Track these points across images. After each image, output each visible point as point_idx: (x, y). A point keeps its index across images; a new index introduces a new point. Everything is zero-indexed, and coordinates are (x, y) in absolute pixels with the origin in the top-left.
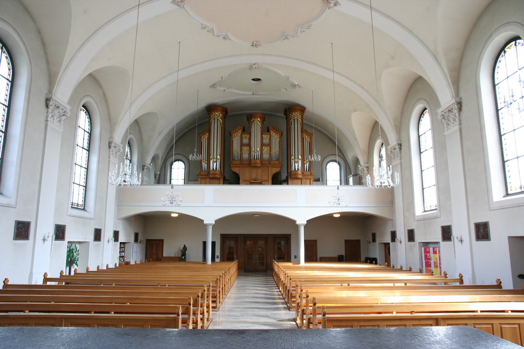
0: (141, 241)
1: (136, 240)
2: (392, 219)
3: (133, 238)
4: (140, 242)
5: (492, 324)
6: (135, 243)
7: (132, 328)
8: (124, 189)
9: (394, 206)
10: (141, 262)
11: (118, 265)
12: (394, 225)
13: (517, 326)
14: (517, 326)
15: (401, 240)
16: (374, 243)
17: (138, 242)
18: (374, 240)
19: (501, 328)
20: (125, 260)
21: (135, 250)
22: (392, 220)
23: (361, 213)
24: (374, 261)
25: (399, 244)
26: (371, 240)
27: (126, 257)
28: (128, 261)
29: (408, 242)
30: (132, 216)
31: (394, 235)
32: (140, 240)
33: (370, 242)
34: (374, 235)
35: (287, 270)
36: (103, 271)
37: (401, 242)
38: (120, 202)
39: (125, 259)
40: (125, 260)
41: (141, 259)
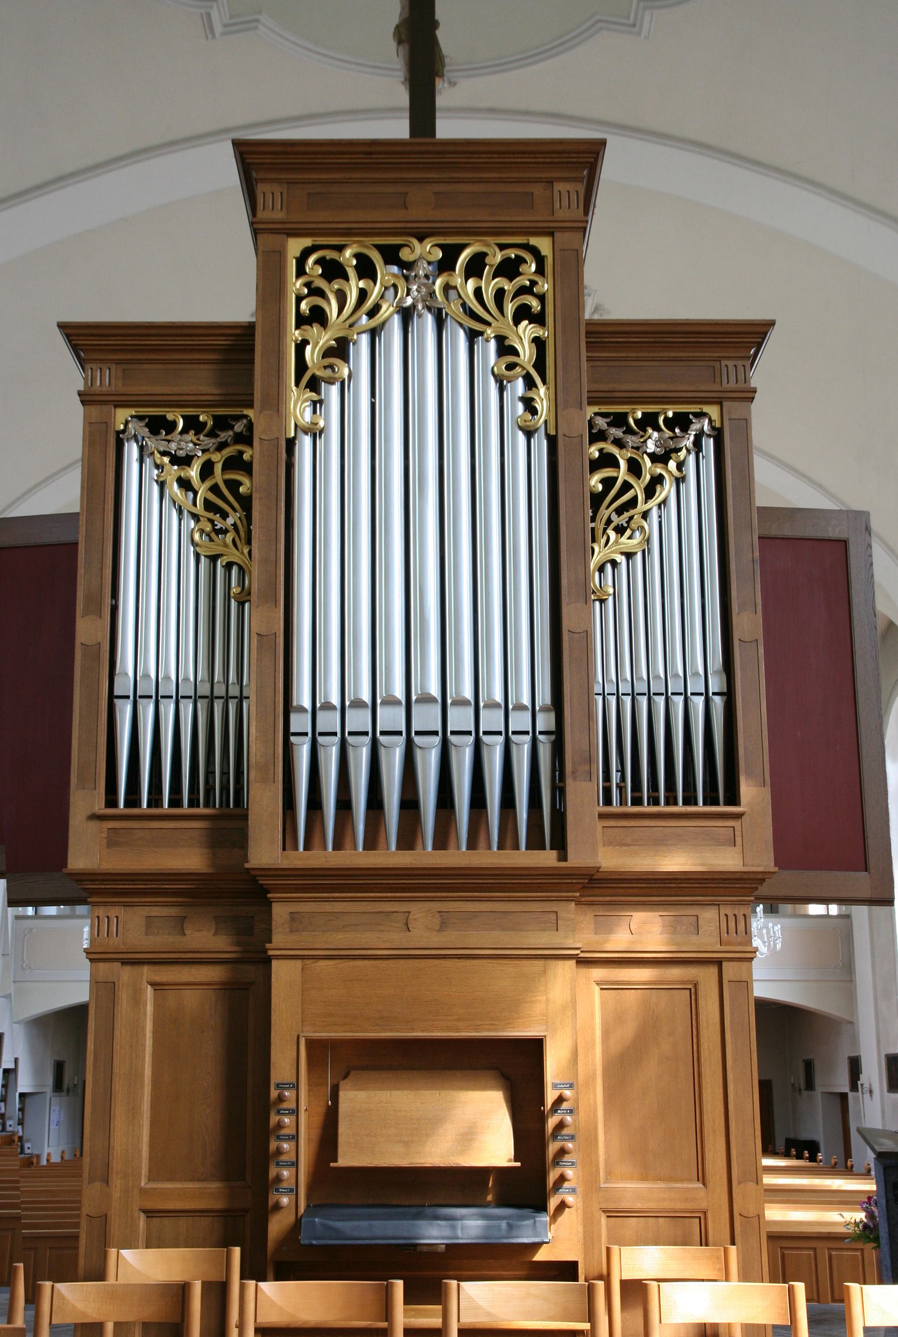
0: (71, 1086)
1: (58, 1086)
2: (851, 1020)
3: (50, 1080)
4: (68, 1091)
5: (815, 1249)
6: (56, 1094)
7: (408, 1034)
8: (34, 930)
9: (853, 979)
10: (62, 1158)
11: (67, 1157)
12: (855, 1040)
13: (859, 1253)
14: (859, 1253)
15: (870, 1085)
16: (810, 1093)
17: (63, 1091)
18: (810, 1085)
19: (830, 1256)
20: (26, 1148)
21: (54, 1118)
22: (851, 1023)
23: (762, 1000)
24: (793, 1150)
25: (867, 1096)
26: (803, 1086)
27: (28, 1141)
28: (35, 1152)
29: (888, 1092)
30: (55, 1011)
31: (855, 1066)
32: (68, 1085)
33: (800, 1090)
34: (809, 1066)
35: (737, 1249)
36: (55, 1165)
37: (871, 1092)
38: (23, 969)
39: (27, 1145)
40: (27, 1151)
41: (62, 1148)
